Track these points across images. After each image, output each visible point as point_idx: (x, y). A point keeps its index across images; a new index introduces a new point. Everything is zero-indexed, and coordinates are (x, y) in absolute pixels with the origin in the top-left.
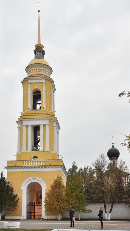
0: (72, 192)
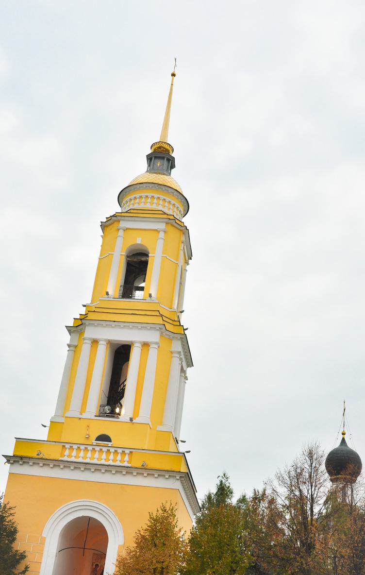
0: (203, 563)
